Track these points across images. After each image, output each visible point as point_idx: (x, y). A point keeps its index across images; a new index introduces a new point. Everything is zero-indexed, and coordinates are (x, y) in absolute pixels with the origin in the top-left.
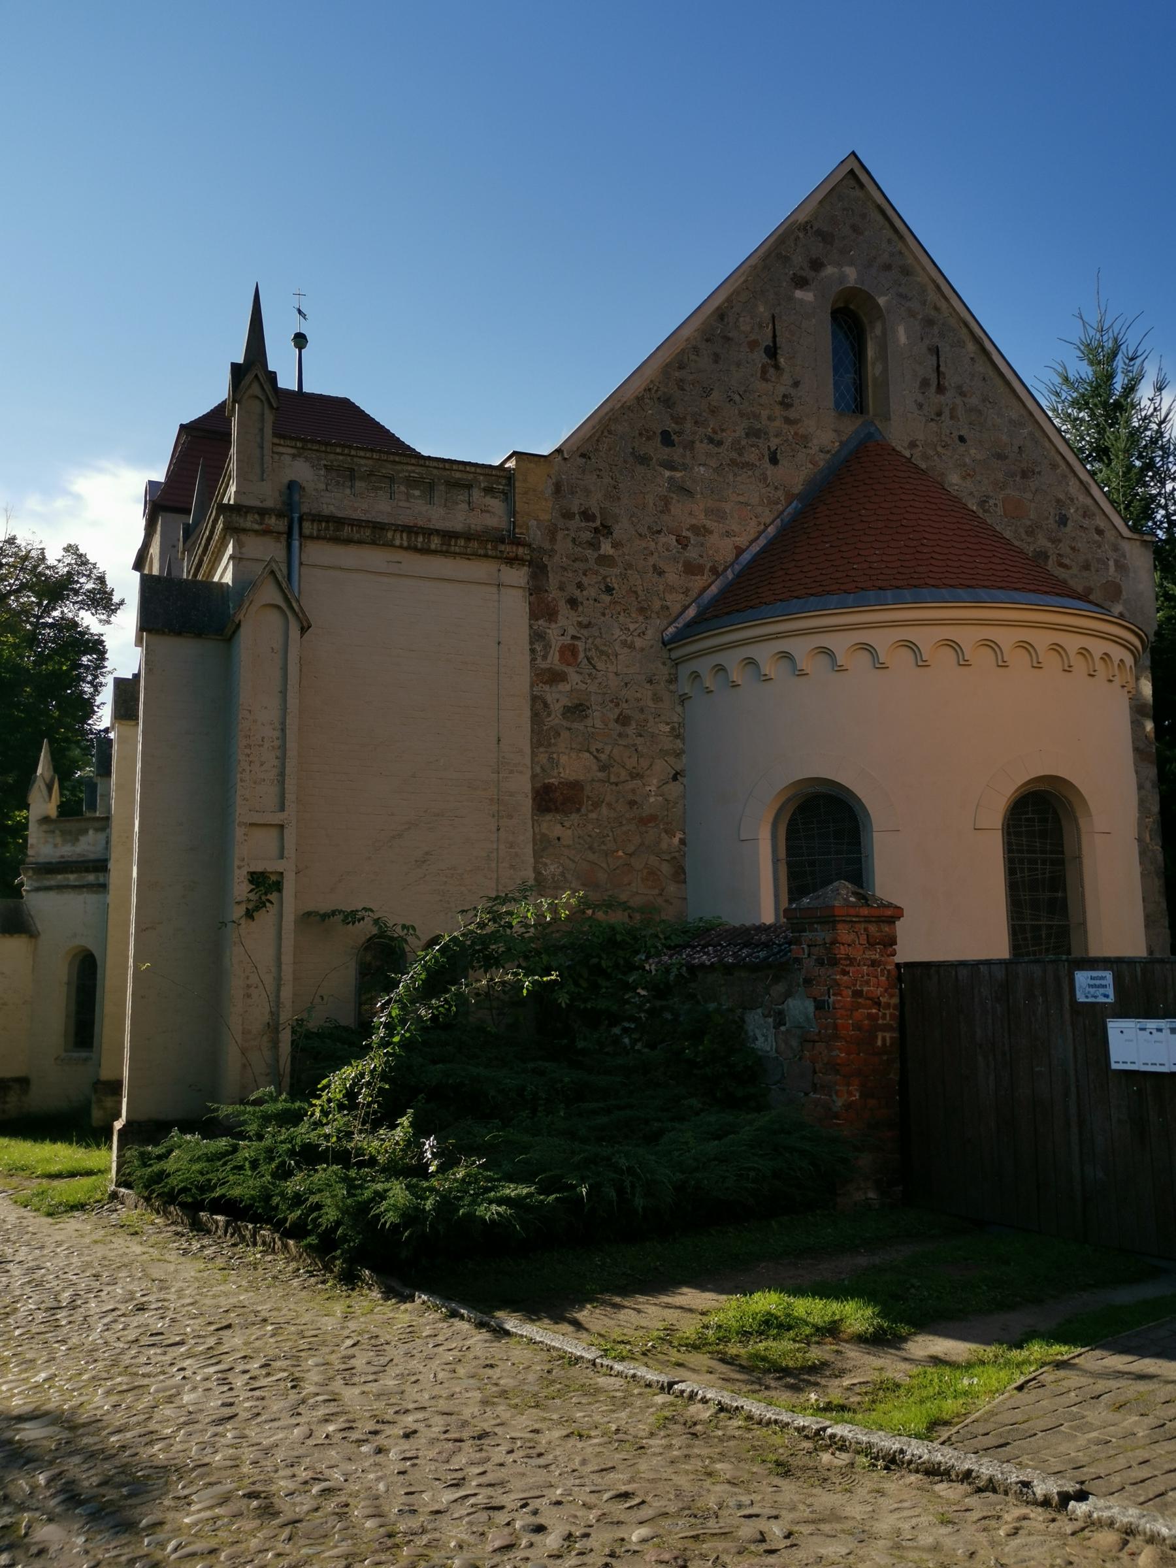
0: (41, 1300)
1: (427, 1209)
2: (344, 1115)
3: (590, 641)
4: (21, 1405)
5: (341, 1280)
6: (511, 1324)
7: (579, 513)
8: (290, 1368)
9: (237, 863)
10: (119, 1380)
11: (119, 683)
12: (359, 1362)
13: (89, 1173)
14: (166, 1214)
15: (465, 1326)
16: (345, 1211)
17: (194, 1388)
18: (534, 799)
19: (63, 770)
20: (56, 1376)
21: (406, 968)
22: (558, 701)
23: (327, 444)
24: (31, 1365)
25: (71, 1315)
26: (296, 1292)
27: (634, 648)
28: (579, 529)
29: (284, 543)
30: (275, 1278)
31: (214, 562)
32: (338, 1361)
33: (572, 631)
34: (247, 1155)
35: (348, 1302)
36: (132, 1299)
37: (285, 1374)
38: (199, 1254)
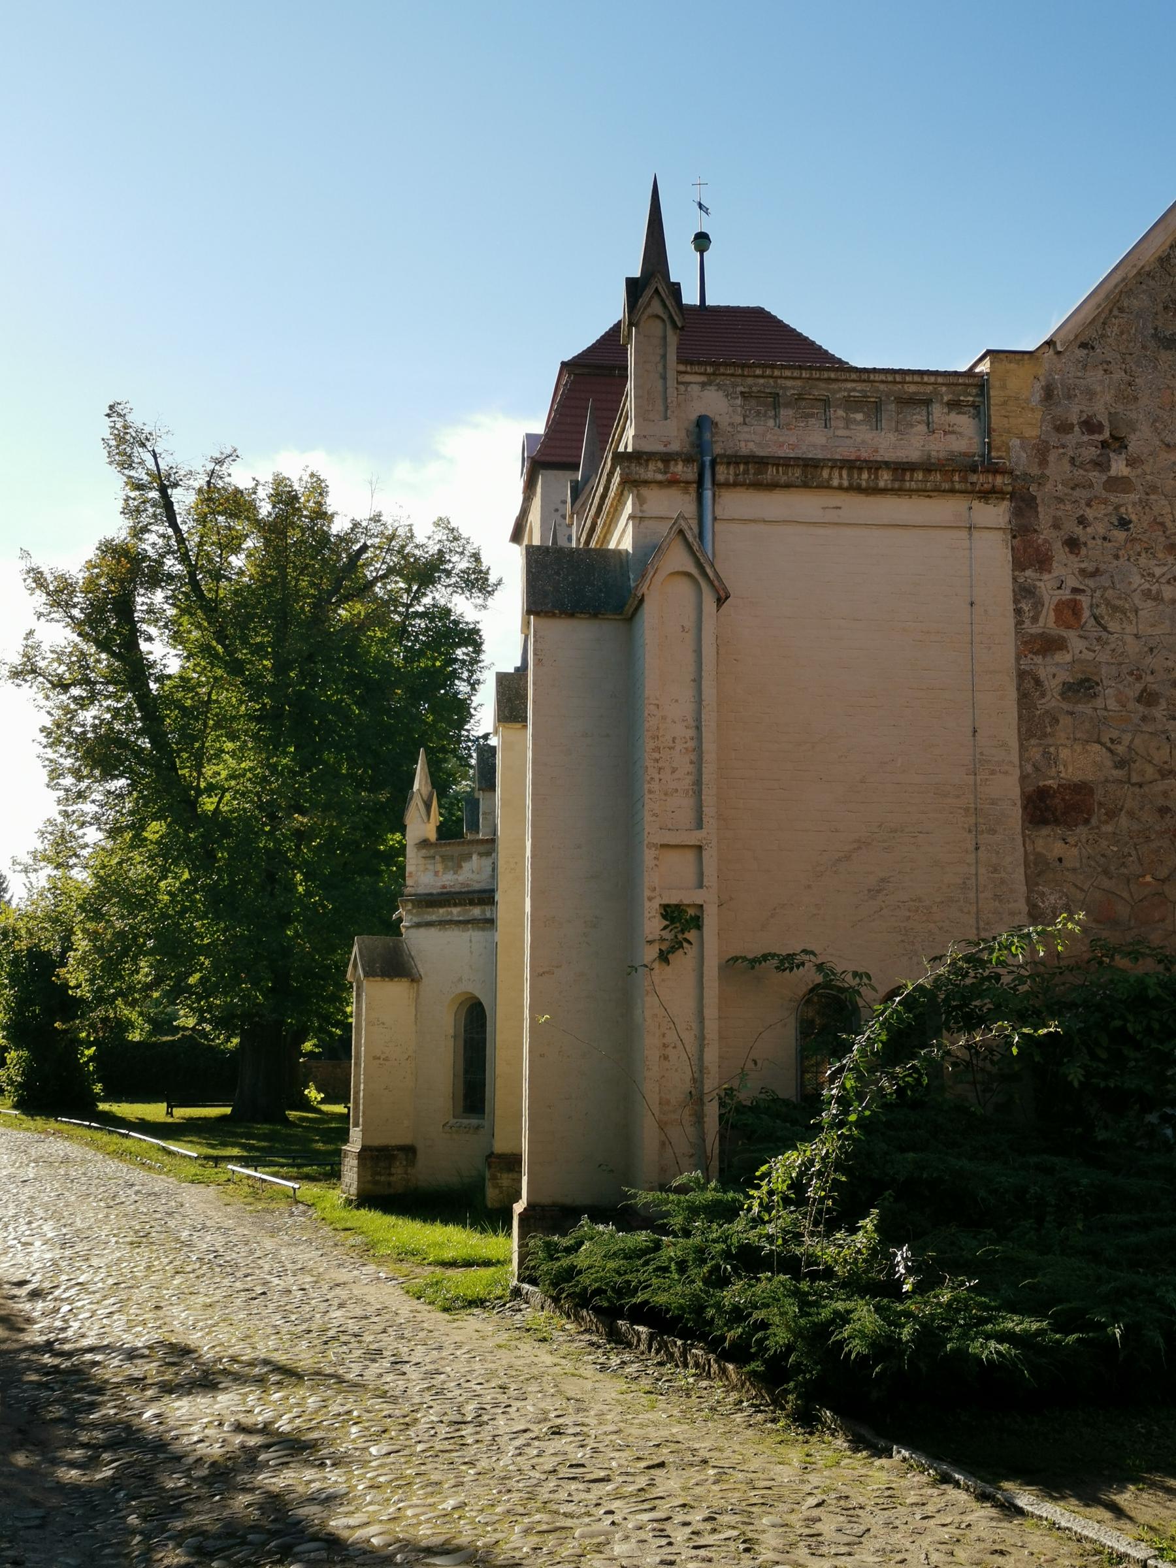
0: (443, 1411)
1: (904, 1339)
2: (792, 1212)
3: (1098, 594)
4: (429, 1536)
5: (795, 1420)
6: (1025, 1501)
7: (1079, 423)
8: (740, 1525)
9: (647, 893)
10: (538, 1517)
11: (502, 678)
12: (827, 1527)
13: (487, 1263)
14: (578, 1319)
15: (961, 1496)
16: (798, 1333)
17: (626, 1538)
18: (1024, 808)
19: (440, 783)
20: (466, 1504)
21: (860, 1026)
22: (1054, 676)
23: (743, 366)
24: (437, 1488)
25: (477, 1433)
26: (740, 1430)
27: (1162, 599)
28: (1079, 445)
29: (694, 495)
30: (713, 1409)
31: (610, 525)
32: (801, 1523)
33: (1072, 582)
34: (672, 1254)
35: (806, 1448)
36: (545, 1420)
37: (735, 1533)
38: (620, 1372)
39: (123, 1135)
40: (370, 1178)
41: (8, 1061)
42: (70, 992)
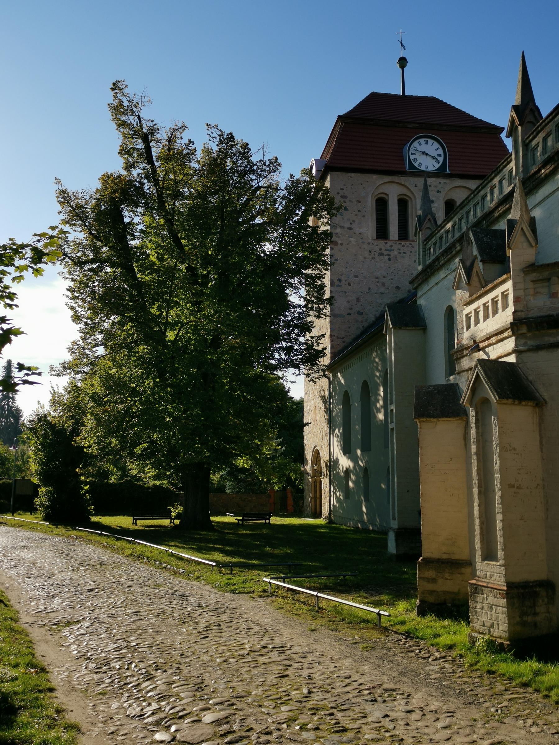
39: (130, 542)
40: (518, 619)
41: (40, 493)
42: (85, 450)
